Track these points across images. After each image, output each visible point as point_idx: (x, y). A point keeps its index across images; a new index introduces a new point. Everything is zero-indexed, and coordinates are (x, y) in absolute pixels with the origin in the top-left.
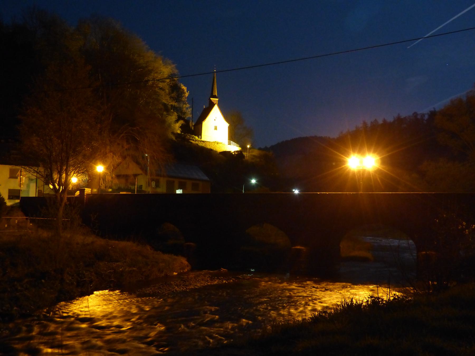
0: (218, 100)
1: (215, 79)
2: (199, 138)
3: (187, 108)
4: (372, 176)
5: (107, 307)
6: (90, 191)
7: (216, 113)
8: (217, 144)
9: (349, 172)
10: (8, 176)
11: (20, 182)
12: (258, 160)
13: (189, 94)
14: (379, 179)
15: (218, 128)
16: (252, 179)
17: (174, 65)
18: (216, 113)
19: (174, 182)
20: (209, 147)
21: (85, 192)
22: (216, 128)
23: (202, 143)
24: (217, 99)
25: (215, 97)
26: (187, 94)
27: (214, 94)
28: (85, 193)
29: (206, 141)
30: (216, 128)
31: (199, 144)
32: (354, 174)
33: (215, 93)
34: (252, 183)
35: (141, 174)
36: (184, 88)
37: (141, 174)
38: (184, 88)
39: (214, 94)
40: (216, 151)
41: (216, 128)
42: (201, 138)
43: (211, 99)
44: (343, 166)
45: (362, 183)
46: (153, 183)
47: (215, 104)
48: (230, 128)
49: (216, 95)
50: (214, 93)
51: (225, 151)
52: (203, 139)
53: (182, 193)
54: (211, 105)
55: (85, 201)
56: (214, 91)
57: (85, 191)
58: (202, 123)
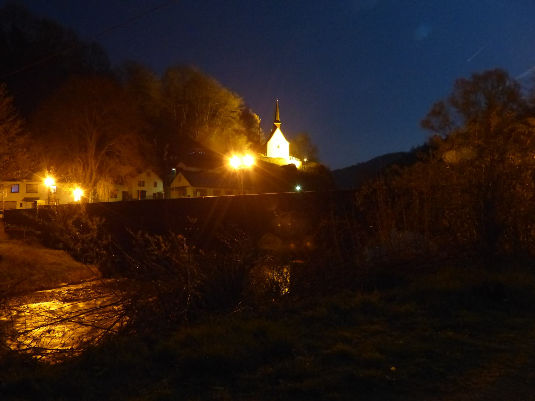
0: (281, 124)
1: (278, 107)
2: (265, 155)
3: (260, 133)
5: (87, 314)
6: (44, 203)
7: (278, 135)
8: (280, 159)
10: (147, 192)
11: (3, 197)
12: (313, 171)
16: (297, 186)
17: (242, 98)
18: (278, 135)
20: (272, 162)
23: (267, 159)
24: (280, 123)
25: (278, 122)
26: (259, 122)
27: (277, 120)
28: (38, 205)
29: (270, 157)
31: (264, 160)
34: (296, 190)
35: (189, 186)
36: (257, 117)
37: (189, 186)
38: (257, 117)
39: (277, 120)
40: (278, 165)
42: (267, 155)
43: (275, 123)
44: (260, 167)
48: (290, 146)
51: (290, 163)
52: (268, 156)
54: (275, 128)
56: (277, 117)
57: (58, 204)
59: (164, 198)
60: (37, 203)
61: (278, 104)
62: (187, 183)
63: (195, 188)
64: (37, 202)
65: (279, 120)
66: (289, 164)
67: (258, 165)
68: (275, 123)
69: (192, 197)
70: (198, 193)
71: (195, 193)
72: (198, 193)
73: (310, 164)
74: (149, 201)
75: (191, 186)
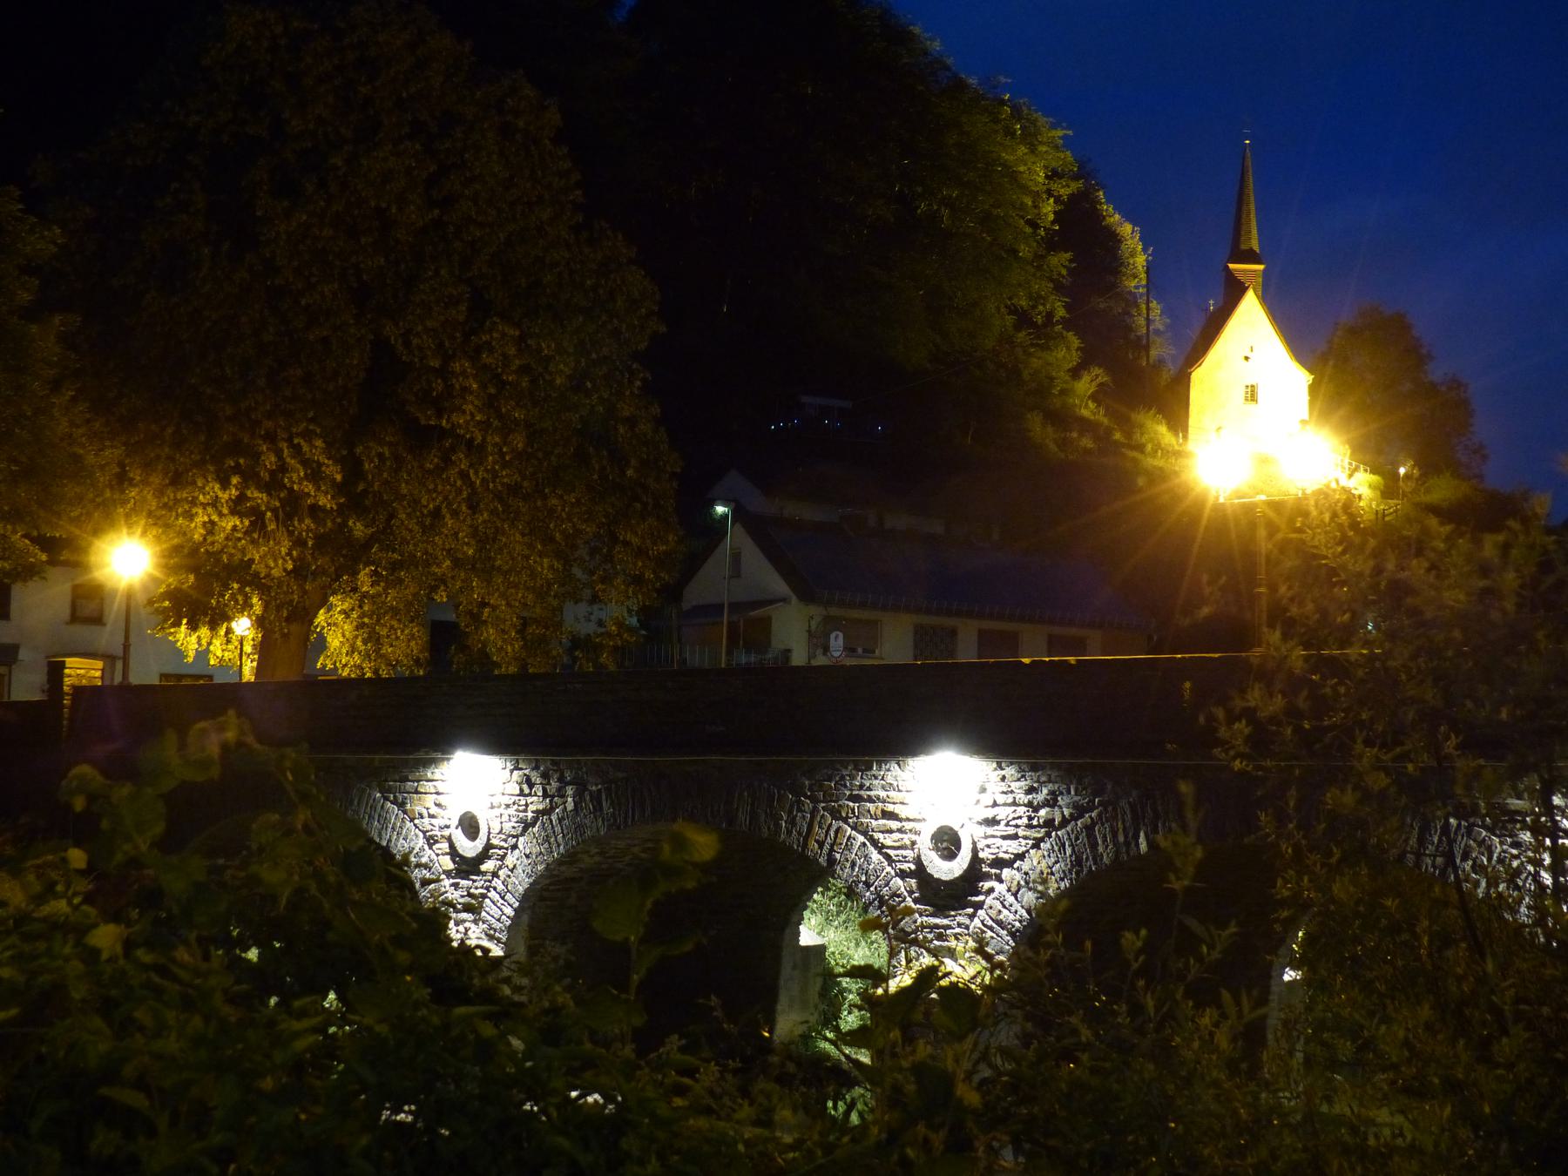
0: (1264, 270)
4: (1207, 512)
6: (98, 674)
9: (1200, 504)
13: (1150, 258)
14: (1202, 529)
15: (1261, 395)
19: (953, 633)
21: (66, 679)
22: (1252, 394)
24: (1261, 267)
25: (1251, 257)
27: (1243, 247)
28: (67, 681)
30: (1252, 394)
32: (1219, 509)
33: (1250, 239)
35: (784, 600)
39: (1243, 247)
41: (1252, 396)
43: (1231, 266)
45: (1262, 590)
46: (837, 637)
47: (1247, 288)
49: (1251, 250)
50: (1243, 233)
53: (253, 680)
54: (1234, 292)
55: (65, 722)
58: (1190, 373)
59: (723, 666)
60: (67, 671)
61: (1249, 162)
62: (780, 586)
63: (816, 611)
64: (62, 665)
65: (1255, 245)
66: (970, 852)
67: (1141, 426)
68: (1231, 266)
69: (799, 659)
70: (837, 642)
71: (818, 640)
72: (837, 642)
73: (884, 825)
74: (116, 686)
75: (794, 599)
